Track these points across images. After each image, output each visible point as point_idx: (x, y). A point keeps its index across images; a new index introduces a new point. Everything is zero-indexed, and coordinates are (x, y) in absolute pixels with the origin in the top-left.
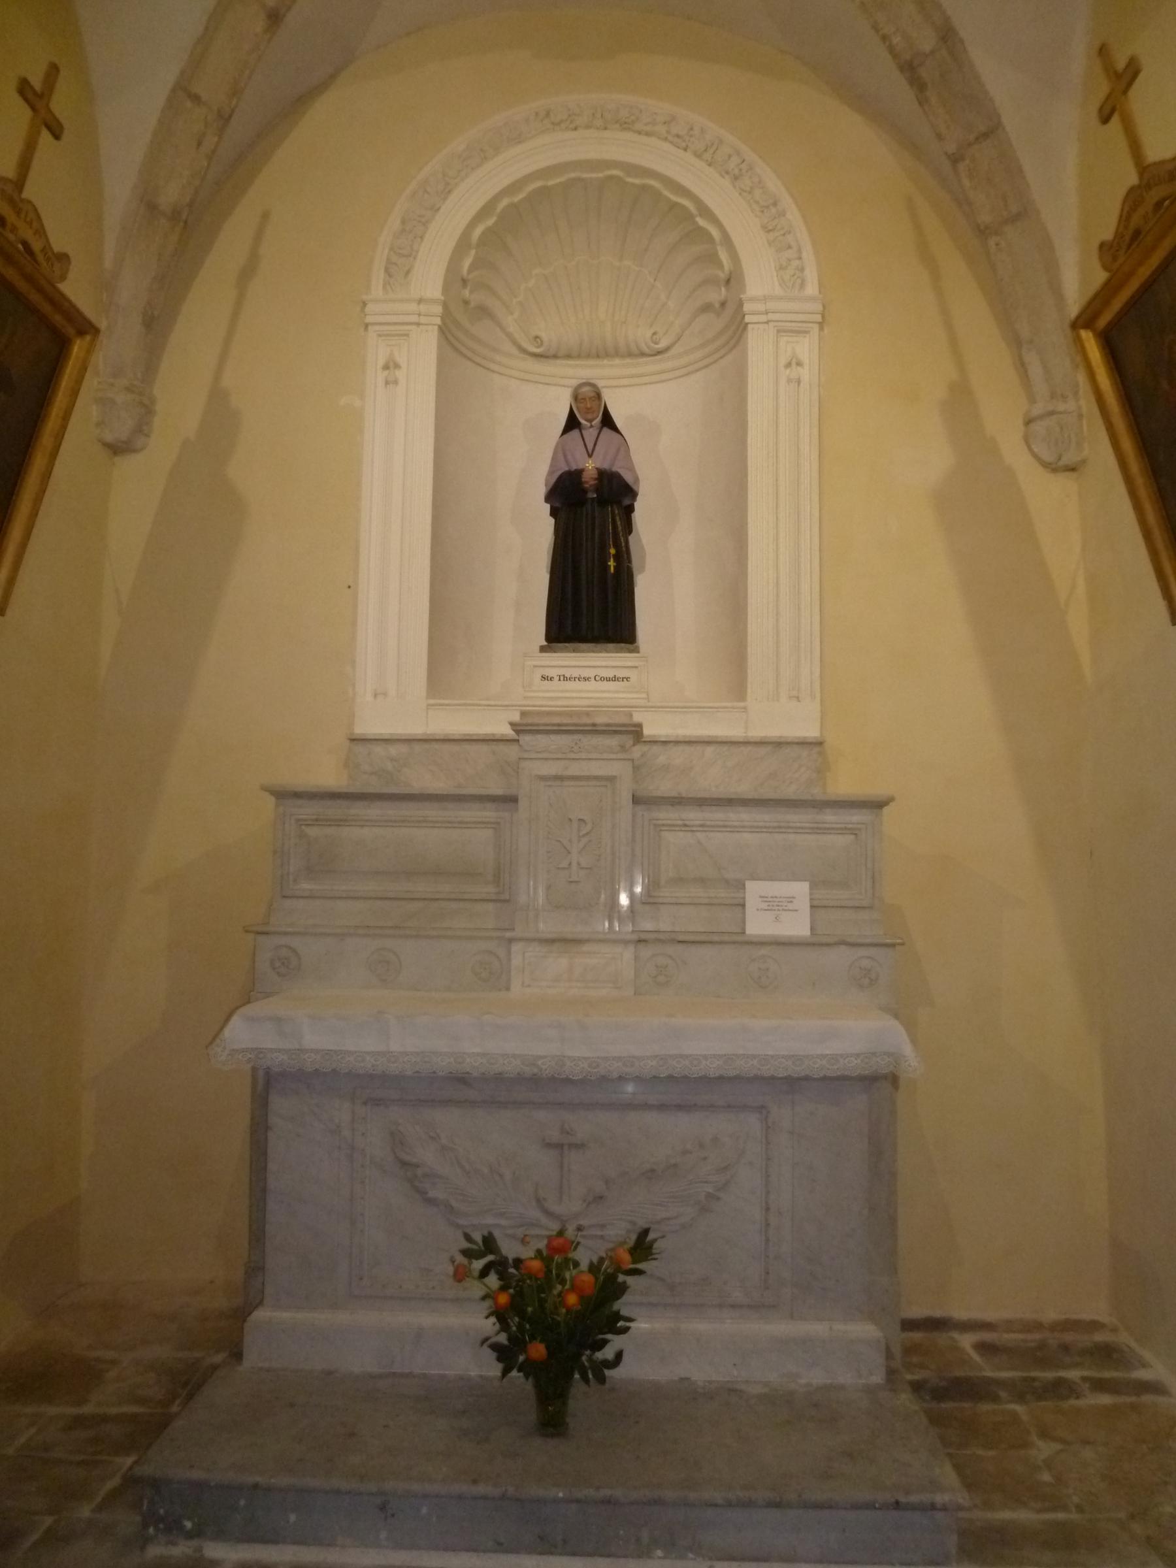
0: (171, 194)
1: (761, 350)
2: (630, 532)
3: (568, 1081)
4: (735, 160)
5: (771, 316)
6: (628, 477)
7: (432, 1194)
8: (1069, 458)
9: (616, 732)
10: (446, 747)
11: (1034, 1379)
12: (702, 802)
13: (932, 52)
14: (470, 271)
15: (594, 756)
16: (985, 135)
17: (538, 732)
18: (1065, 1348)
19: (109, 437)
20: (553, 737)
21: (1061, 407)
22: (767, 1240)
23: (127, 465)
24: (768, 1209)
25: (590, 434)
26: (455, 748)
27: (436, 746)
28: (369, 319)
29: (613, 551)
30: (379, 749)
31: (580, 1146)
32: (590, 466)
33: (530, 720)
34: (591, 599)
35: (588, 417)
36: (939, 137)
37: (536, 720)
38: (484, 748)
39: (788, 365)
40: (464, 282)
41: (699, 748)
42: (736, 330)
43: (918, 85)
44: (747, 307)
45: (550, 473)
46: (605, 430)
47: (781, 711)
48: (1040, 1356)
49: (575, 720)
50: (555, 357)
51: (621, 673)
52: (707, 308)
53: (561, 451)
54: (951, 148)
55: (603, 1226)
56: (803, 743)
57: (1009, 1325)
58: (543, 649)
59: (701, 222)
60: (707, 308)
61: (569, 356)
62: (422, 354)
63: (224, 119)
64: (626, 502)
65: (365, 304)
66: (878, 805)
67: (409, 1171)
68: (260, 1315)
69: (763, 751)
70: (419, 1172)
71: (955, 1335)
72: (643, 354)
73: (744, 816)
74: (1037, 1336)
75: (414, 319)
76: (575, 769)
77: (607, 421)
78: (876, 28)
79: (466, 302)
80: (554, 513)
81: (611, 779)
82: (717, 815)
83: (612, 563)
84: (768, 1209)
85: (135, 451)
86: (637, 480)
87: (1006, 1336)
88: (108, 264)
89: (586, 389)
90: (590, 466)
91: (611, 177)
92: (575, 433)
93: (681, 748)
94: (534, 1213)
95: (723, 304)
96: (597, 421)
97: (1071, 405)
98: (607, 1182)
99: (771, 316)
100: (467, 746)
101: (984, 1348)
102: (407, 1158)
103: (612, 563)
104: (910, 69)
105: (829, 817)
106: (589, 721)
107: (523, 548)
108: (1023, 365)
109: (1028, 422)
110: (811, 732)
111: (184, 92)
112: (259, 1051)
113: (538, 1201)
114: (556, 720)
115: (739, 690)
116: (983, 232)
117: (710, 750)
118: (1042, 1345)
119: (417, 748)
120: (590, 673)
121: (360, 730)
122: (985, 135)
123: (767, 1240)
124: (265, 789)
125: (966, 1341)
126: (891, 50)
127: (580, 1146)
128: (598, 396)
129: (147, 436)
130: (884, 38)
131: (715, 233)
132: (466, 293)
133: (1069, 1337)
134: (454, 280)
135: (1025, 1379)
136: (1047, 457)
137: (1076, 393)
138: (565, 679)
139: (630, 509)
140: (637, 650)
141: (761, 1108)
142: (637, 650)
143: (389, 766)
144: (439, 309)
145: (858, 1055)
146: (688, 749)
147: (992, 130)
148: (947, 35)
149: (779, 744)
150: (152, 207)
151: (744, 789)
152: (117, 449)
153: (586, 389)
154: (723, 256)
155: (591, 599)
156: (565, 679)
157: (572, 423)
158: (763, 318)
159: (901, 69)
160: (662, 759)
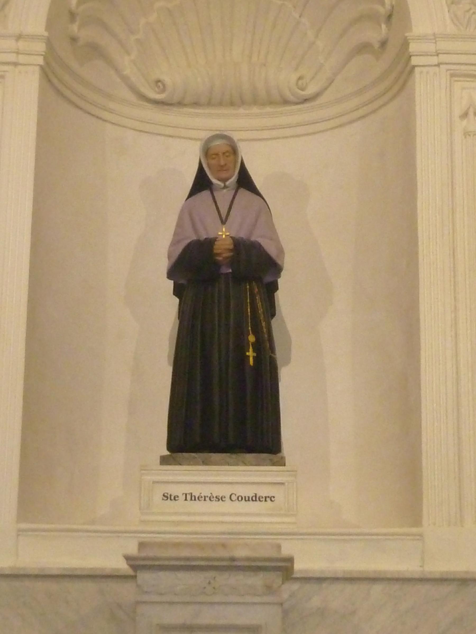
5: (443, 58)
10: (40, 585)
17: (161, 568)
20: (181, 575)
25: (223, 197)
26: (53, 586)
29: (252, 338)
32: (224, 234)
34: (225, 399)
35: (221, 176)
38: (90, 586)
44: (413, 47)
45: (174, 243)
50: (180, 104)
51: (263, 492)
52: (363, 48)
53: (187, 216)
58: (164, 461)
60: (363, 48)
61: (196, 104)
64: (268, 279)
69: (445, 589)
77: (245, 181)
80: (178, 291)
83: (251, 353)
86: (281, 251)
90: (224, 234)
92: (206, 194)
96: (234, 179)
99: (443, 58)
103: (251, 353)
107: (141, 334)
114: (185, 553)
117: (377, 589)
128: (234, 151)
138: (193, 498)
139: (273, 287)
153: (218, 142)
155: (225, 399)
157: (201, 183)
158: (435, 60)
160: (316, 602)
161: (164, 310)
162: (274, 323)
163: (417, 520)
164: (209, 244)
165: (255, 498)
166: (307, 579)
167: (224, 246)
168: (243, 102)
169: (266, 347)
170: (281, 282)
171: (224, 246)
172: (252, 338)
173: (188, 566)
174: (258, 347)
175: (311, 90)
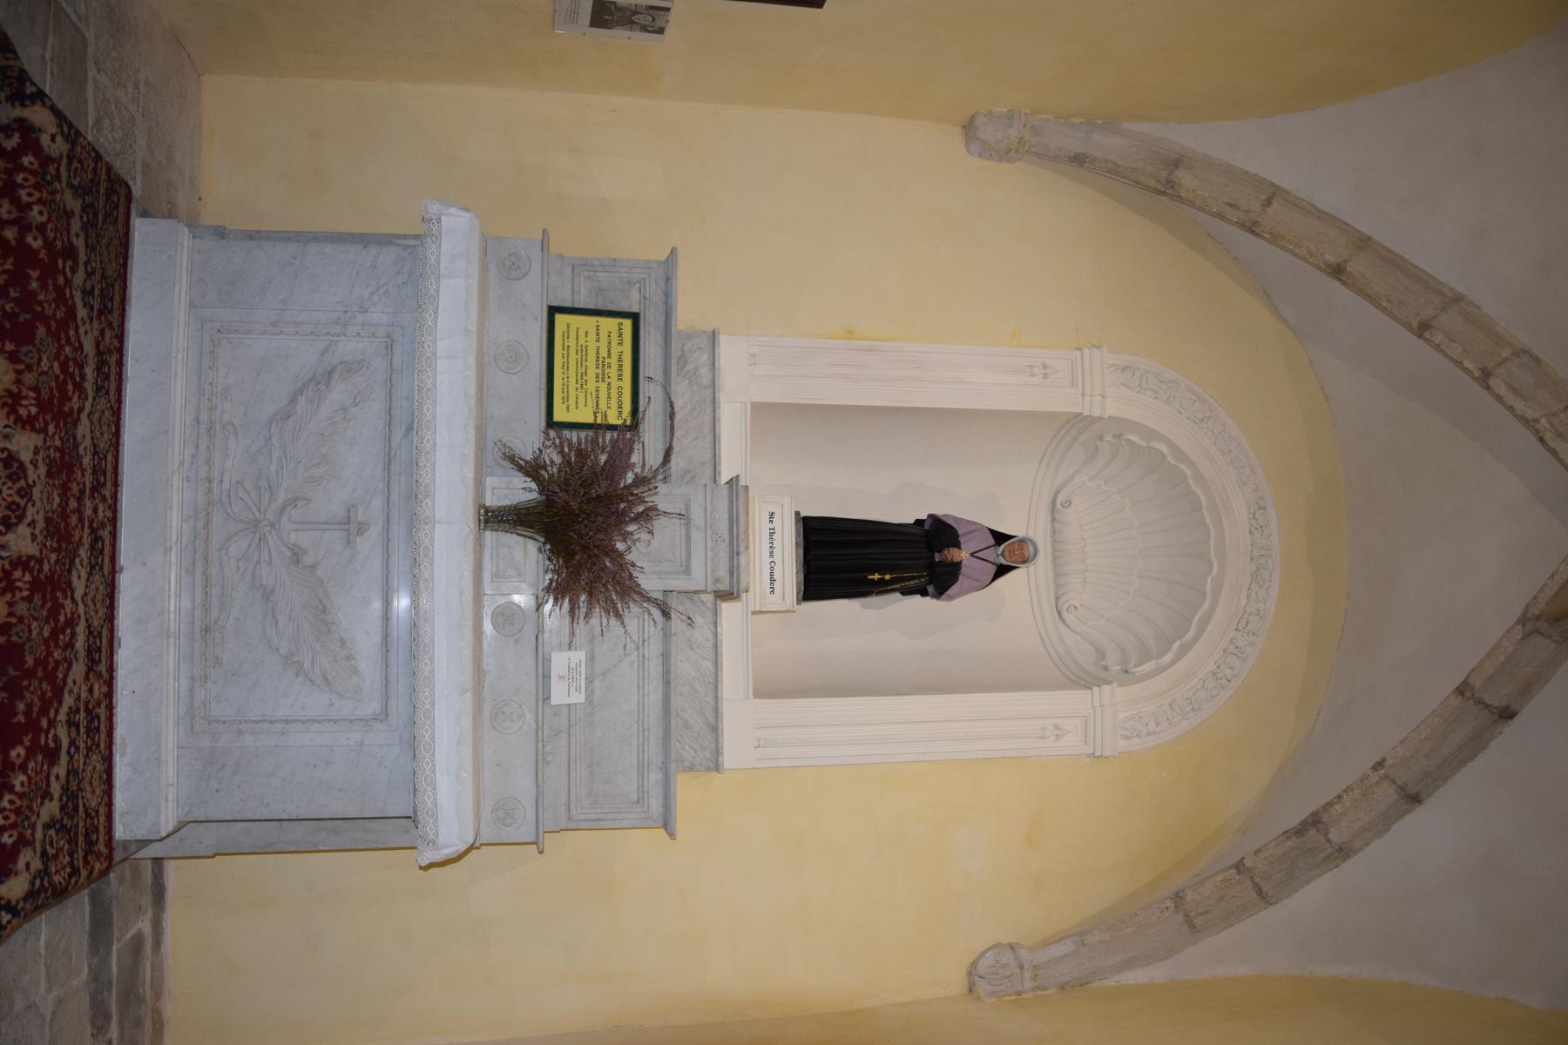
0: (1185, 179)
1: (1073, 701)
2: (903, 594)
3: (412, 528)
4: (1229, 673)
5: (1099, 710)
6: (953, 590)
7: (302, 400)
8: (983, 987)
9: (732, 574)
10: (708, 419)
11: (110, 992)
12: (666, 656)
13: (1329, 840)
14: (1129, 441)
15: (709, 554)
16: (1260, 892)
17: (731, 502)
18: (138, 1023)
19: (979, 121)
20: (726, 516)
21: (1027, 975)
22: (256, 722)
23: (956, 139)
24: (287, 722)
25: (990, 554)
26: (707, 428)
27: (709, 410)
28: (1086, 351)
29: (888, 577)
30: (705, 358)
31: (349, 543)
32: (963, 555)
33: (741, 494)
34: (843, 559)
35: (1006, 556)
36: (1257, 852)
37: (741, 500)
38: (708, 456)
39: (1057, 727)
40: (1119, 436)
41: (712, 655)
42: (1085, 680)
43: (1300, 831)
44: (1106, 688)
45: (956, 519)
46: (994, 568)
47: (747, 727)
48: (130, 995)
49: (742, 536)
50: (1053, 520)
51: (777, 585)
52: (1101, 654)
53: (976, 527)
54: (1248, 863)
55: (270, 564)
56: (718, 752)
57: (158, 967)
58: (797, 513)
59: (1176, 646)
60: (1101, 654)
61: (1054, 532)
62: (1063, 400)
63: (1252, 228)
64: (930, 589)
65: (1100, 347)
66: (667, 824)
67: (323, 378)
68: (185, 234)
69: (710, 716)
70: (322, 387)
71: (150, 914)
72: (1057, 599)
73: (654, 697)
74: (148, 994)
75: (1088, 392)
76: (697, 537)
77: (1002, 570)
78: (1348, 790)
79: (1101, 438)
80: (919, 522)
81: (687, 571)
82: (654, 669)
83: (877, 576)
84: (287, 722)
85: (967, 144)
86: (951, 598)
87: (148, 965)
88: (1125, 125)
89: (1031, 549)
90: (963, 555)
91: (1211, 564)
92: (991, 541)
93: (711, 638)
94: (281, 497)
95: (1106, 668)
96: (1004, 562)
97: (1028, 984)
98: (313, 566)
99: (1099, 710)
100: (709, 438)
101: (138, 941)
102: (336, 376)
103: (877, 576)
104: (1314, 821)
105: (655, 777)
106: (742, 548)
107: (886, 496)
108: (1062, 939)
109: (1011, 947)
110: (728, 761)
111: (1272, 194)
112: (438, 238)
113: (296, 500)
114: (742, 519)
115: (765, 690)
116: (1178, 897)
117: (709, 665)
118: (140, 1000)
119: (708, 393)
120: (777, 557)
121: (723, 340)
122: (1260, 892)
123: (256, 722)
124: (673, 251)
125: (144, 925)
126: (1330, 804)
127: (349, 543)
128: (1025, 561)
129: (980, 155)
130: (1340, 797)
131: (1167, 659)
132: (1108, 438)
133: (148, 1025)
134: (1120, 427)
135: (110, 983)
136: (982, 967)
137: (1039, 988)
138: (772, 534)
139: (924, 593)
140: (799, 603)
141: (385, 713)
142: (799, 603)
143: (689, 367)
144: (1096, 413)
145: (435, 804)
146: (710, 644)
147: (1264, 898)
148: (1344, 852)
149: (715, 730)
150: (1176, 164)
151: (677, 702)
152: (969, 129)
153: (1031, 549)
154: (1148, 667)
155: (843, 559)
156: (772, 534)
157: (1000, 538)
158: (1097, 704)
159: (1314, 814)
160: (698, 620)
161: (903, 512)
162: (897, 595)
163: (759, 694)
164: (958, 545)
165: (772, 580)
166: (716, 613)
167: (954, 554)
168: (1056, 567)
169: (881, 588)
170: (928, 599)
171: (954, 554)
172: (888, 577)
173: (733, 521)
174: (882, 582)
175: (1067, 616)
